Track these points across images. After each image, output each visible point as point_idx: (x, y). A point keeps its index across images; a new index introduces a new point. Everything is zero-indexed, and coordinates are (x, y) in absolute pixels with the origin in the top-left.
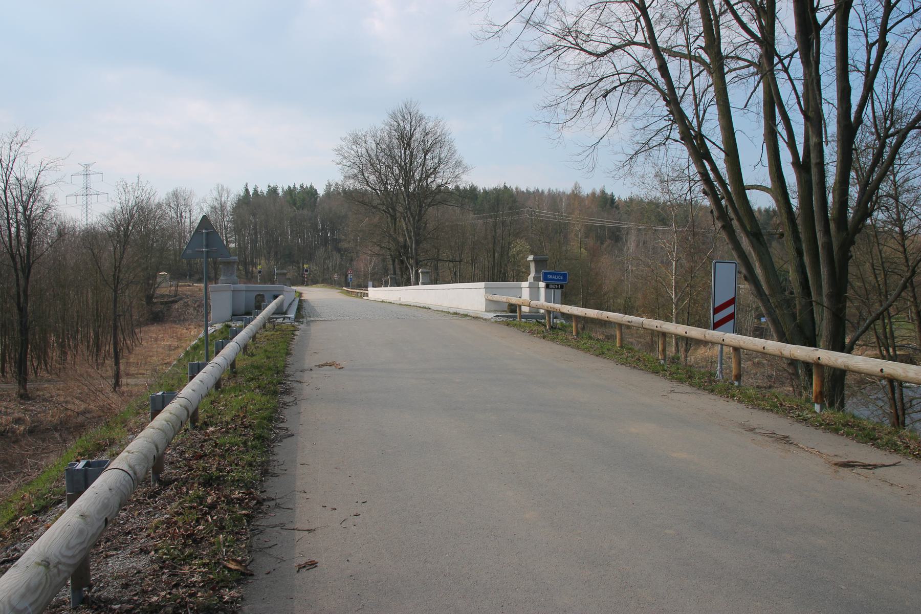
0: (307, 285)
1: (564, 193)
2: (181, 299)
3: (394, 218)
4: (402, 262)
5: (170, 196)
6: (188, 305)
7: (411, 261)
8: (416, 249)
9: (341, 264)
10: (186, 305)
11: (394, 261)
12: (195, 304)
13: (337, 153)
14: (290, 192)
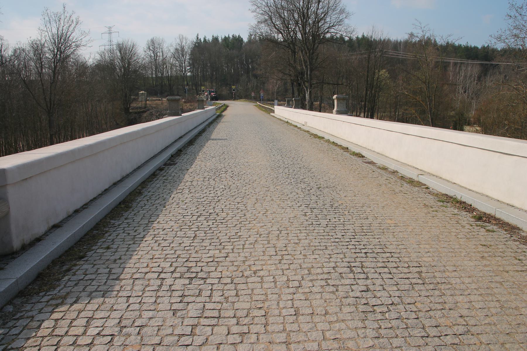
1: (389, 41)
2: (148, 110)
3: (294, 52)
4: (299, 85)
5: (150, 42)
6: (152, 114)
7: (306, 84)
8: (310, 75)
9: (257, 85)
11: (293, 84)
12: (157, 114)
13: (252, 4)
14: (226, 39)
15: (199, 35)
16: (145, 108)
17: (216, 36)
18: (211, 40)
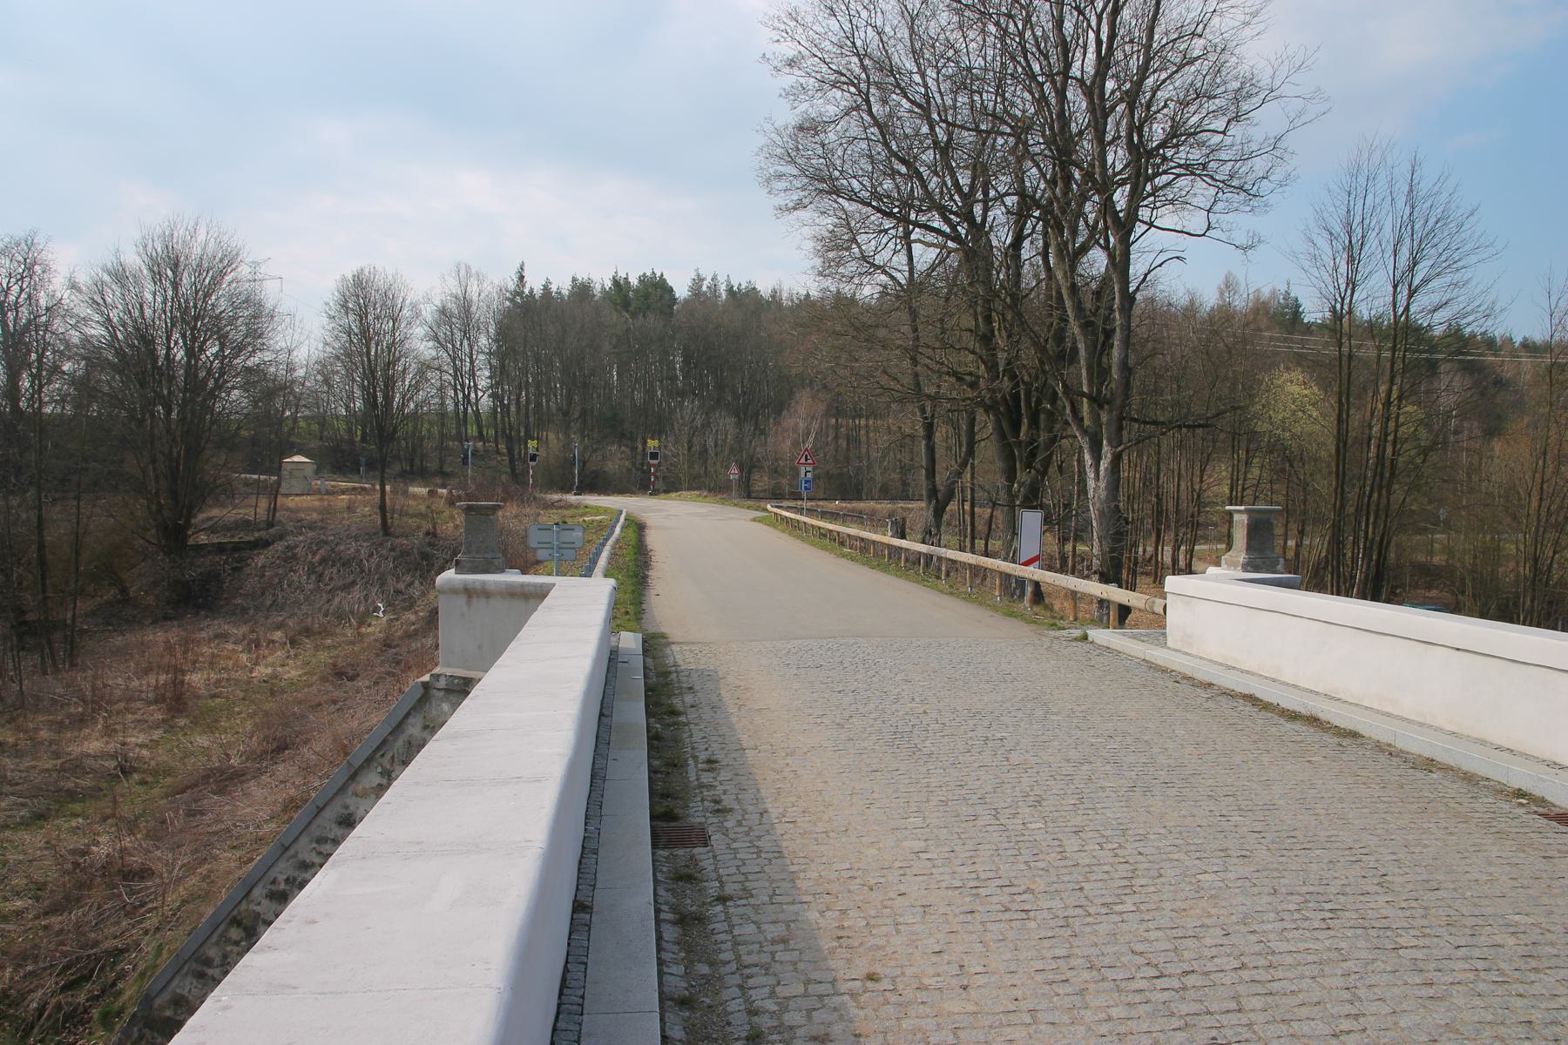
0: (655, 493)
2: (281, 537)
6: (294, 557)
10: (290, 558)
12: (314, 554)
14: (619, 285)
15: (525, 269)
16: (270, 525)
17: (586, 278)
18: (566, 292)
